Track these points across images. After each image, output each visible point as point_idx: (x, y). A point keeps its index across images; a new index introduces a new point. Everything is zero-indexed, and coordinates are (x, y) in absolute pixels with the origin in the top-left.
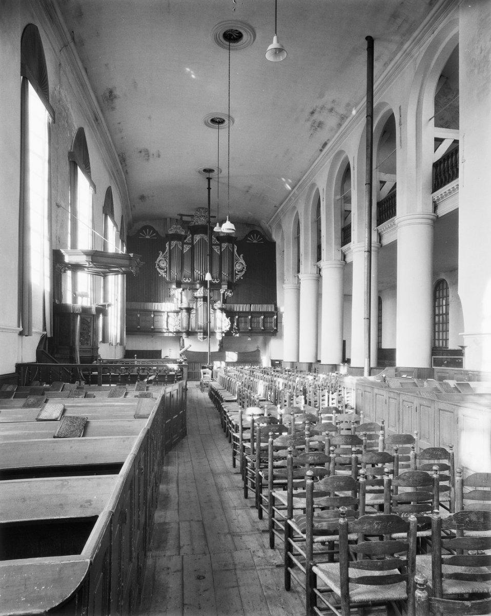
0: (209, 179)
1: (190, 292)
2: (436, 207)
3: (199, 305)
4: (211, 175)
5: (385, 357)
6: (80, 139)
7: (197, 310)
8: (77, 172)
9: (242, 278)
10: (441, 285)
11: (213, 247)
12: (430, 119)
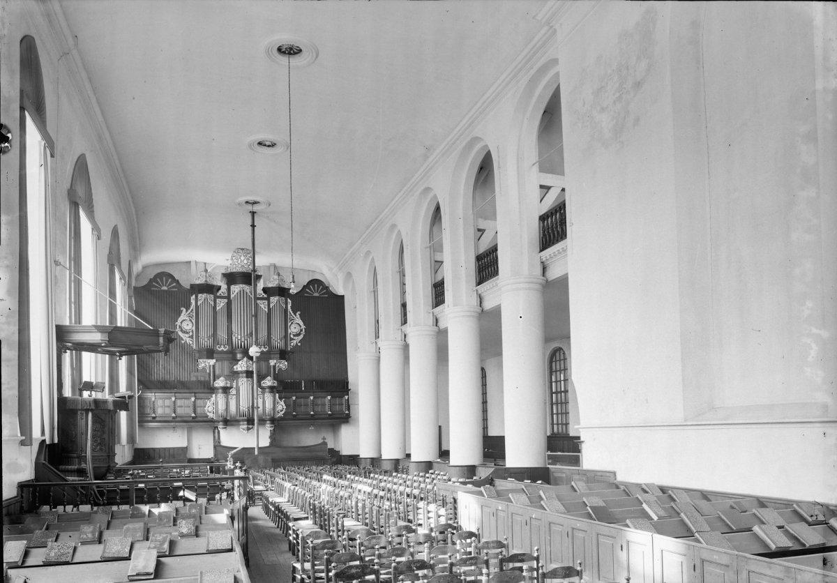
0: (253, 213)
1: (226, 364)
2: (544, 269)
3: (240, 383)
4: (256, 208)
5: (493, 448)
6: (81, 167)
7: (238, 390)
8: (79, 216)
9: (299, 344)
10: (557, 354)
11: (258, 302)
12: (534, 164)
